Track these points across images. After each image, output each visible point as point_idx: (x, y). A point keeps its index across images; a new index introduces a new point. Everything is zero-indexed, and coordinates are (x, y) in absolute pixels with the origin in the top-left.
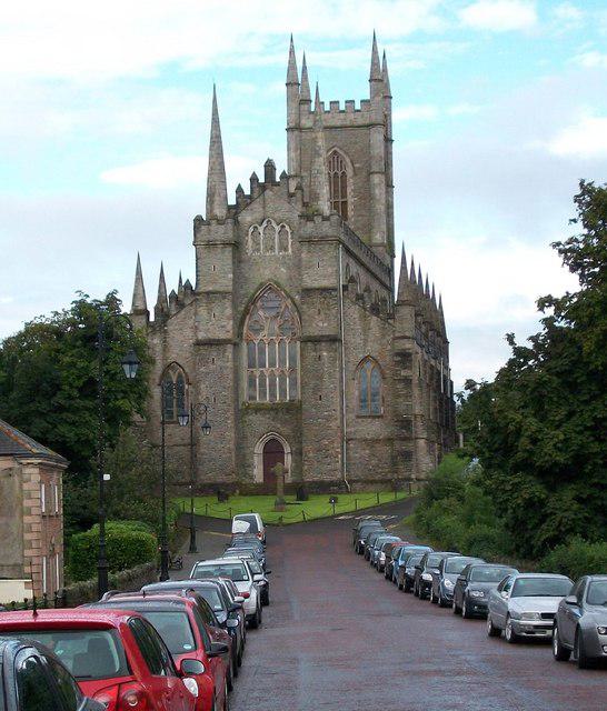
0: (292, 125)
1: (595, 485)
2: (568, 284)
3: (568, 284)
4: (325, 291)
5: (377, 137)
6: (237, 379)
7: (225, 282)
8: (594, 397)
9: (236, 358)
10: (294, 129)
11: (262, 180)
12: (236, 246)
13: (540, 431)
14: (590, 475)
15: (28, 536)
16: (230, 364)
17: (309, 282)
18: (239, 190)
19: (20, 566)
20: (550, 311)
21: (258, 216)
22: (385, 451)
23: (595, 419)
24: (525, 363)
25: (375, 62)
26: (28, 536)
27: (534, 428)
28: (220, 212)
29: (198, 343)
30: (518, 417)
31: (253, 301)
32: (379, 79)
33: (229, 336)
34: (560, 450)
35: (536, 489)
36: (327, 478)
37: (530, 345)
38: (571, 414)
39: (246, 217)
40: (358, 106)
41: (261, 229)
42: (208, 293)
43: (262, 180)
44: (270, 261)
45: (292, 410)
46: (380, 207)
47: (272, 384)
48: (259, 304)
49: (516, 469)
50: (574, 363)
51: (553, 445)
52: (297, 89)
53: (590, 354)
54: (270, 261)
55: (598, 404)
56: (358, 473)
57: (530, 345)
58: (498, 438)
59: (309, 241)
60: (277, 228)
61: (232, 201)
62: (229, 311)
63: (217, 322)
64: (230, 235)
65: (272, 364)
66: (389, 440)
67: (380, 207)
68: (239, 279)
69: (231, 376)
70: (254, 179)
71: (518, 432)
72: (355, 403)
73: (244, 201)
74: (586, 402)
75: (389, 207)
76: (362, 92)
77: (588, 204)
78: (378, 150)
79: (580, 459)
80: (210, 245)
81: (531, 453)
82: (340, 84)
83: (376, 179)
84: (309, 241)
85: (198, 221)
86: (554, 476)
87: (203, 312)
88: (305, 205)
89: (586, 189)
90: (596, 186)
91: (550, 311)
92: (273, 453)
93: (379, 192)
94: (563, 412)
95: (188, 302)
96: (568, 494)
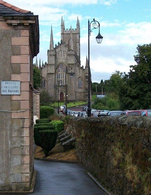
0: (62, 33)
1: (141, 99)
2: (135, 63)
3: (135, 63)
4: (72, 64)
5: (78, 36)
6: (55, 81)
7: (54, 62)
8: (140, 84)
9: (55, 77)
10: (62, 34)
11: (60, 43)
12: (55, 56)
13: (131, 90)
14: (139, 98)
15: (37, 108)
16: (54, 78)
17: (69, 63)
18: (56, 45)
19: (36, 113)
20: (132, 68)
21: (59, 50)
22: (83, 94)
23: (140, 88)
24: (127, 77)
25: (62, 22)
26: (37, 108)
27: (130, 89)
28: (52, 49)
29: (48, 74)
30: (127, 87)
31: (58, 66)
32: (78, 25)
33: (54, 72)
34: (135, 93)
35: (130, 100)
36: (72, 99)
37: (128, 74)
38: (136, 87)
39: (57, 50)
40: (74, 30)
41: (60, 52)
42: (50, 64)
43: (60, 43)
44: (62, 59)
45: (66, 86)
46: (78, 49)
47: (64, 81)
48: (59, 66)
49: (126, 97)
50: (137, 78)
51: (134, 91)
52: (63, 25)
53: (140, 76)
54: (62, 59)
55: (141, 85)
56: (78, 98)
57: (128, 74)
58: (123, 91)
59: (69, 55)
60: (63, 52)
61: (55, 47)
62: (54, 68)
63: (52, 70)
64: (54, 53)
65: (62, 78)
66: (84, 93)
67: (78, 49)
68: (56, 62)
69: (54, 80)
70: (59, 43)
71: (127, 90)
72: (77, 85)
73: (57, 47)
74: (139, 85)
75: (80, 49)
76: (74, 27)
77: (139, 49)
78: (78, 38)
79: (138, 95)
80: (50, 55)
81: (130, 94)
82: (70, 25)
83: (78, 44)
84: (69, 55)
85: (48, 51)
86: (134, 98)
87: (49, 68)
88: (68, 48)
89: (139, 46)
90: (141, 46)
91: (132, 68)
92: (62, 94)
93: (78, 46)
94: (135, 86)
95: (46, 66)
96: (136, 101)
